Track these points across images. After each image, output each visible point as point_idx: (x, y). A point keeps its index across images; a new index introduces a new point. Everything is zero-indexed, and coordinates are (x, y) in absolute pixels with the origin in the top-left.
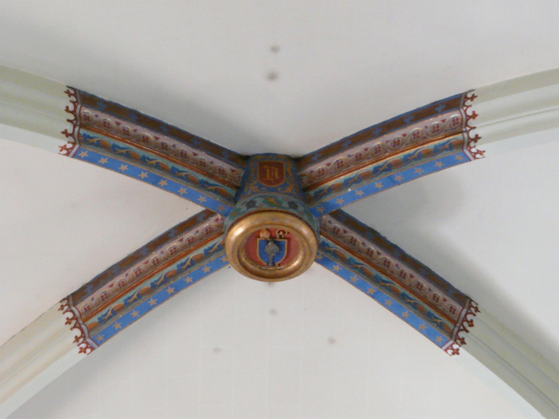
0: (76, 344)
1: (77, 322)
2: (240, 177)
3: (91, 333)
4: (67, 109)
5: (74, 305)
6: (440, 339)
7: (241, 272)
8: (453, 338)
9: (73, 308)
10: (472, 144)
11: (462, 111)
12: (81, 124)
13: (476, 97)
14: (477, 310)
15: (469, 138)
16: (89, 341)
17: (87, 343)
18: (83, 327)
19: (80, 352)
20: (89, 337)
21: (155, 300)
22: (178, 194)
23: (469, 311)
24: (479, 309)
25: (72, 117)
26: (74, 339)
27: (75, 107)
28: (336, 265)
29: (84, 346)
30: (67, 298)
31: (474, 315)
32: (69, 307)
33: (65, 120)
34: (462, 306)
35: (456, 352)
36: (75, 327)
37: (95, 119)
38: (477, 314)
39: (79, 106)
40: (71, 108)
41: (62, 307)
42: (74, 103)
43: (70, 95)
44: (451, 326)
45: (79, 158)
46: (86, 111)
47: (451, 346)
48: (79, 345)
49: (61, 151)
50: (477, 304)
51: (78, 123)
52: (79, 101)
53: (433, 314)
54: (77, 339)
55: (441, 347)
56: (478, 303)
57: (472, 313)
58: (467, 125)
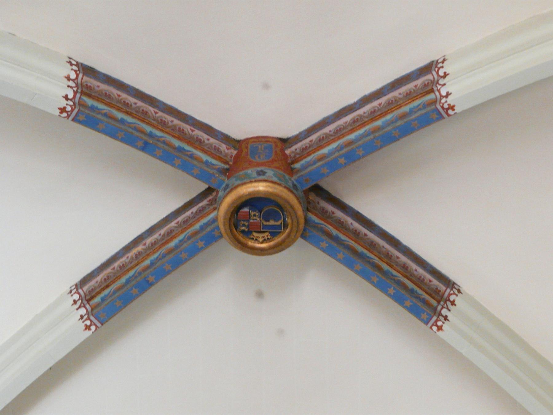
0: (81, 321)
1: (82, 302)
2: (232, 156)
3: (94, 311)
4: (68, 78)
5: (81, 288)
6: (425, 316)
7: (236, 246)
8: (437, 314)
9: (80, 291)
10: (443, 100)
11: (434, 73)
12: (82, 91)
13: (448, 74)
14: (459, 291)
15: (441, 96)
16: (92, 318)
17: (91, 321)
18: (88, 306)
19: (86, 329)
20: (92, 315)
21: (154, 277)
22: (173, 165)
23: (452, 292)
24: (462, 291)
25: (71, 84)
26: (79, 317)
27: (77, 76)
28: (323, 241)
29: (88, 323)
30: (76, 285)
31: (457, 295)
32: (77, 290)
33: (66, 86)
34: (429, 73)
35: (440, 328)
36: (80, 307)
37: (96, 89)
38: (460, 295)
39: (81, 75)
40: (73, 76)
41: (71, 292)
42: (76, 71)
43: (71, 64)
44: (434, 303)
45: (80, 122)
46: (90, 102)
47: (436, 321)
48: (83, 322)
49: (61, 113)
50: (459, 287)
51: (79, 90)
52: (81, 70)
53: (416, 291)
54: (82, 317)
55: (427, 323)
56: (444, 55)
57: (454, 294)
58: (438, 82)
